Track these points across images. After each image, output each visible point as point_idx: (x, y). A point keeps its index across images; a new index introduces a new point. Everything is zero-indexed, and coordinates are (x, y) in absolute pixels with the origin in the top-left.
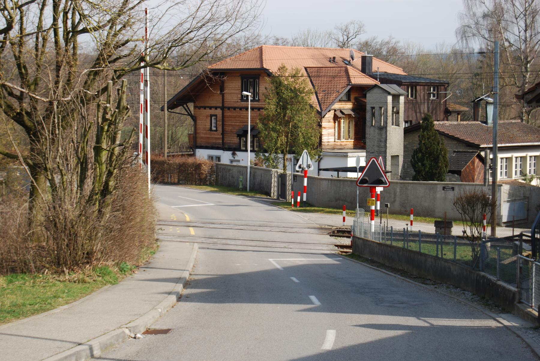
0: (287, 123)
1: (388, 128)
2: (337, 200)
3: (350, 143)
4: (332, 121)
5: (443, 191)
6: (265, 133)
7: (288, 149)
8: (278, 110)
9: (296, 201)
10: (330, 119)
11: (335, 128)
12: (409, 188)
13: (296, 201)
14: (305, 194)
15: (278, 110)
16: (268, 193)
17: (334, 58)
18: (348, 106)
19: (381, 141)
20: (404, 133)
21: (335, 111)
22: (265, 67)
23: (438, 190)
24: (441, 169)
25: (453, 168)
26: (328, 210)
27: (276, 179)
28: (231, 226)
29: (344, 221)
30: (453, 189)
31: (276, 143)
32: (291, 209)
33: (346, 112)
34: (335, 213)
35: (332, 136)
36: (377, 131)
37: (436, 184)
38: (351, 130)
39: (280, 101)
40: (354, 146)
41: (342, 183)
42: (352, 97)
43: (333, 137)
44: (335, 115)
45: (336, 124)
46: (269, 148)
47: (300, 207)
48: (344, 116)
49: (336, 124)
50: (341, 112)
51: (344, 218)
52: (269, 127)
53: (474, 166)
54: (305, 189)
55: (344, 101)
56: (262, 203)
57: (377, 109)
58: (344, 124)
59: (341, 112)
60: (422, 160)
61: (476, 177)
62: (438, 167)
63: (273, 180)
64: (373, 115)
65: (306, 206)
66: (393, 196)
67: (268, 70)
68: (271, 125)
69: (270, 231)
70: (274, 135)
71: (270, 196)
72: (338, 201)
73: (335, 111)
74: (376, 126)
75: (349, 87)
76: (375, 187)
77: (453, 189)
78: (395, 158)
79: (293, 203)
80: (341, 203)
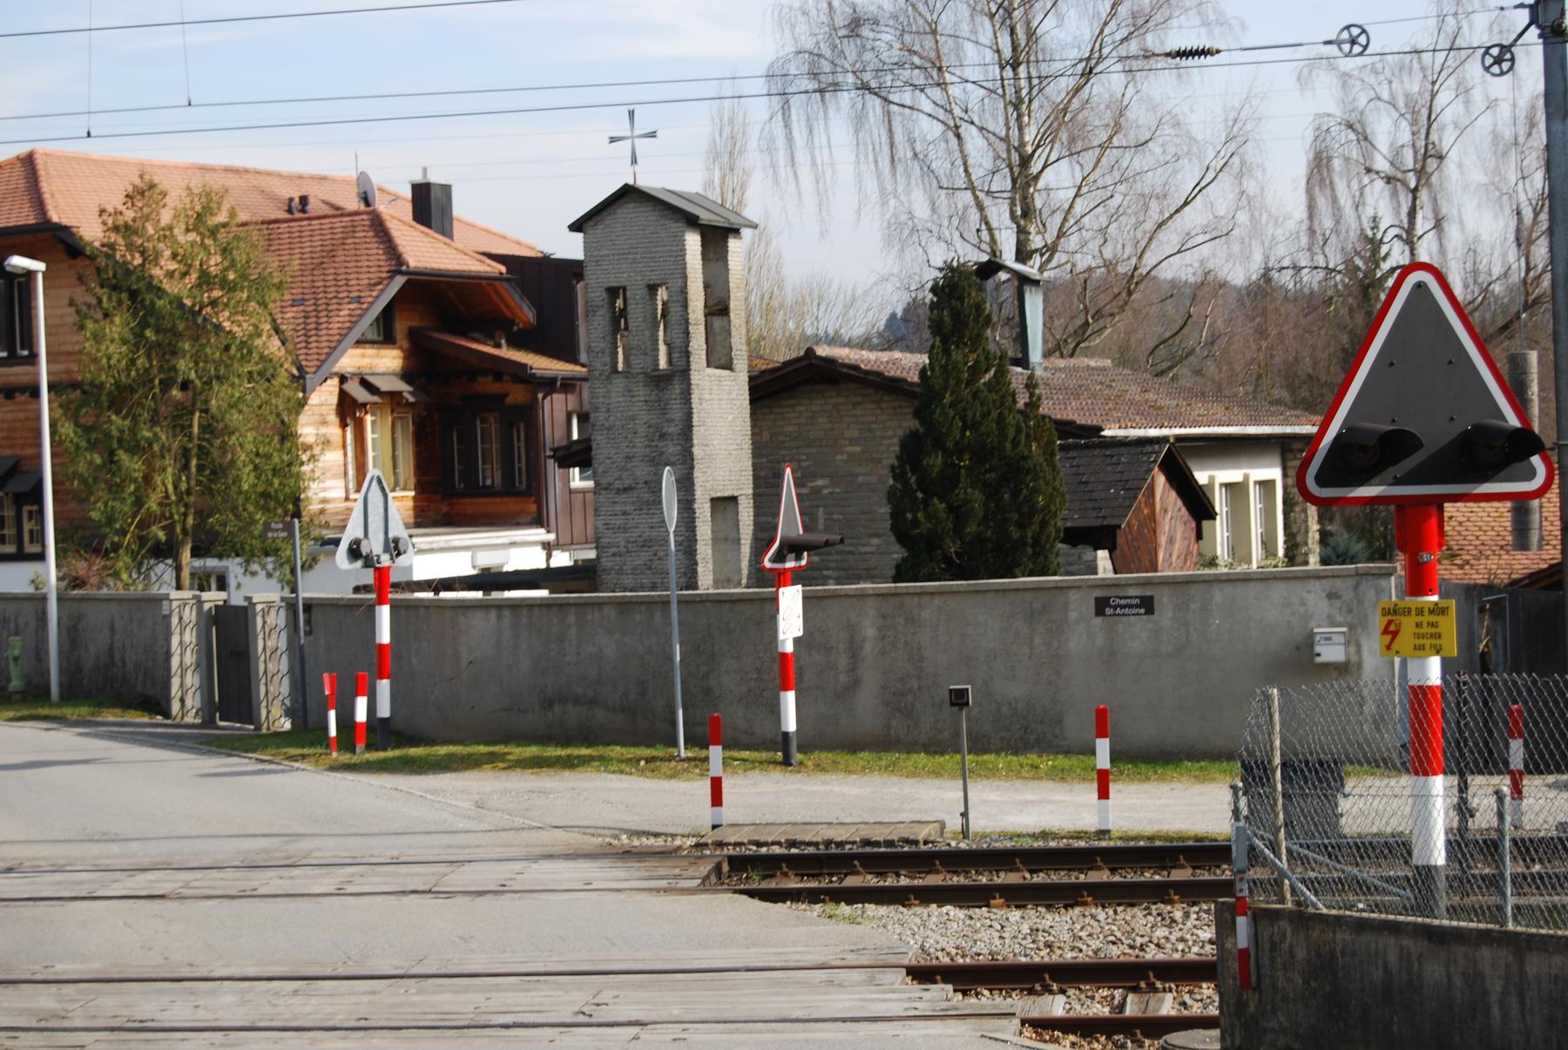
0: (179, 419)
1: (695, 378)
2: (548, 703)
3: (403, 502)
4: (333, 418)
5: (1099, 620)
6: (91, 463)
7: (190, 521)
8: (142, 362)
9: (346, 721)
10: (324, 410)
11: (344, 446)
12: (926, 614)
13: (346, 721)
14: (384, 686)
15: (142, 362)
16: (156, 703)
17: (304, 200)
18: (386, 362)
19: (663, 436)
20: (752, 402)
21: (343, 379)
22: (55, 219)
23: (1073, 615)
24: (1044, 524)
25: (1077, 520)
26: (517, 752)
27: (190, 637)
28: (87, 882)
29: (717, 800)
30: (1147, 605)
31: (139, 502)
32: (326, 761)
33: (385, 385)
34: (569, 764)
35: (334, 477)
36: (641, 392)
37: (1059, 588)
38: (399, 453)
39: (144, 325)
40: (416, 516)
41: (571, 618)
42: (401, 327)
43: (342, 483)
44: (344, 397)
45: (349, 430)
46: (110, 520)
47: (370, 747)
48: (376, 399)
49: (349, 430)
50: (365, 384)
51: (716, 784)
52: (108, 435)
53: (1153, 506)
54: (383, 663)
55: (372, 343)
56: (154, 745)
57: (636, 293)
58: (376, 430)
59: (365, 384)
60: (944, 485)
61: (1161, 556)
62: (1033, 510)
63: (175, 640)
64: (618, 320)
65: (397, 743)
66: (843, 661)
67: (66, 229)
68: (117, 423)
69: (339, 893)
70: (132, 465)
71: (166, 714)
72: (557, 708)
73: (343, 379)
74: (637, 369)
75: (400, 281)
76: (1439, 501)
77: (1147, 605)
78: (724, 504)
79: (333, 732)
80: (574, 713)
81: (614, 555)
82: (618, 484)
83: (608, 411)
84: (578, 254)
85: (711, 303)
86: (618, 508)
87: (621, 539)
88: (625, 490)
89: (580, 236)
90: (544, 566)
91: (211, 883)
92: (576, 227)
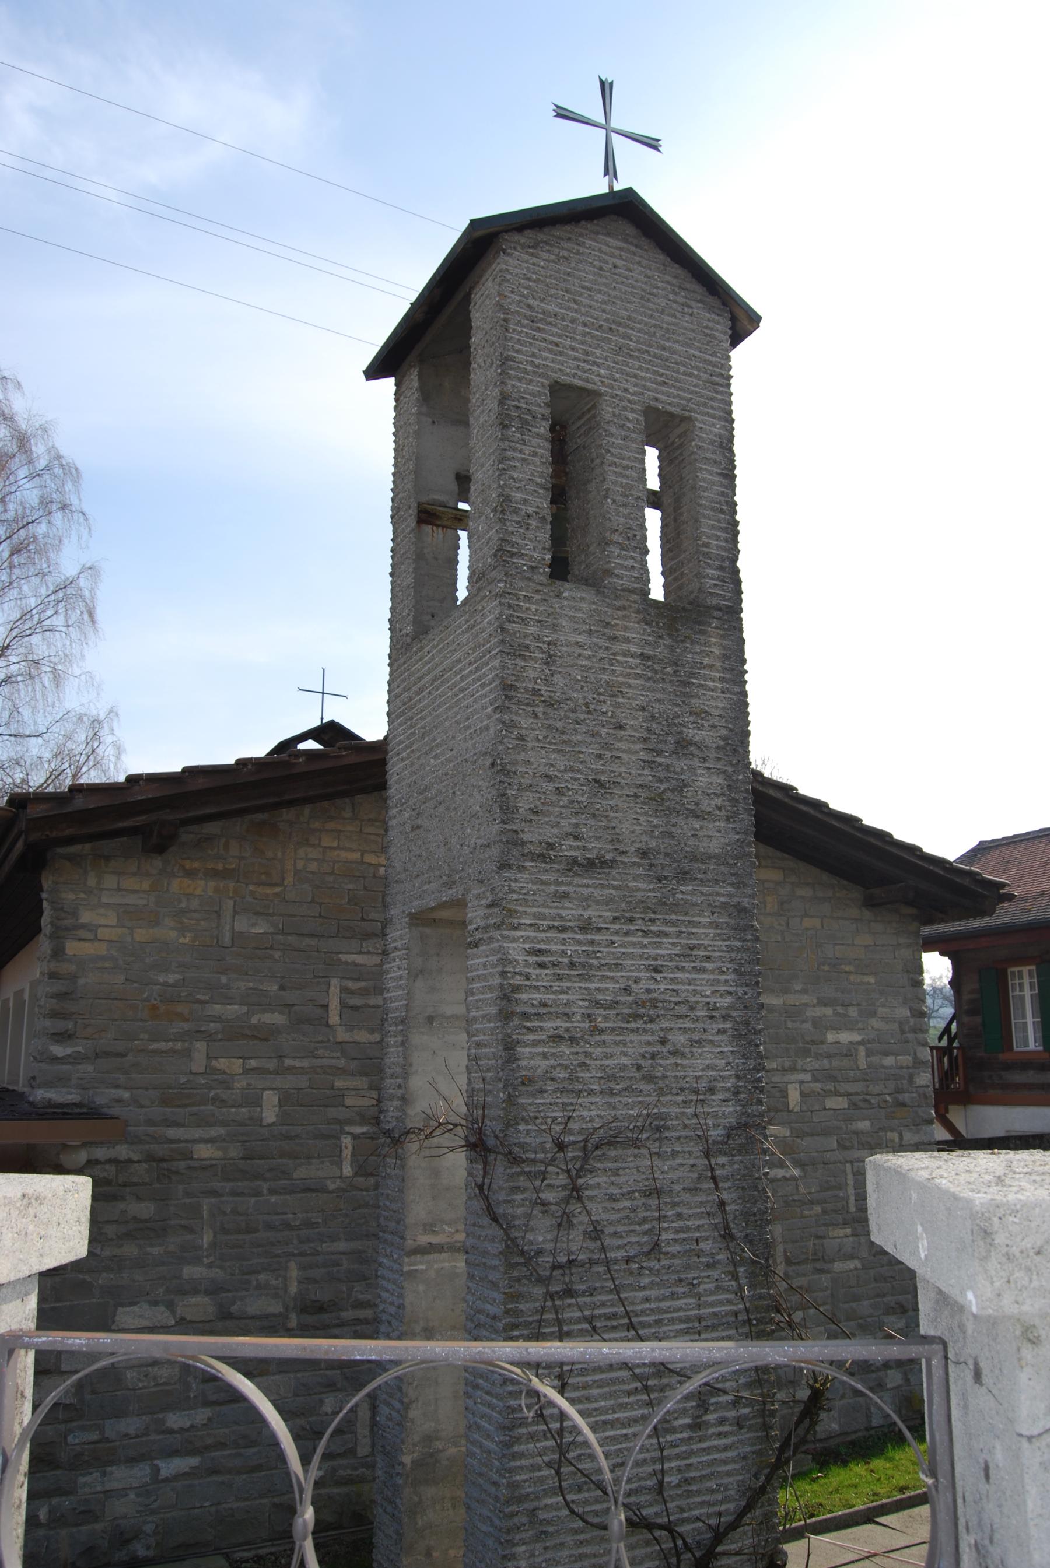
19: (683, 745)
81: (556, 1038)
82: (569, 849)
83: (549, 660)
84: (33, 1351)
85: (716, 644)
86: (570, 911)
87: (574, 994)
88: (593, 865)
89: (388, 385)
90: (606, 190)
91: (936, 1399)
92: (375, 371)
